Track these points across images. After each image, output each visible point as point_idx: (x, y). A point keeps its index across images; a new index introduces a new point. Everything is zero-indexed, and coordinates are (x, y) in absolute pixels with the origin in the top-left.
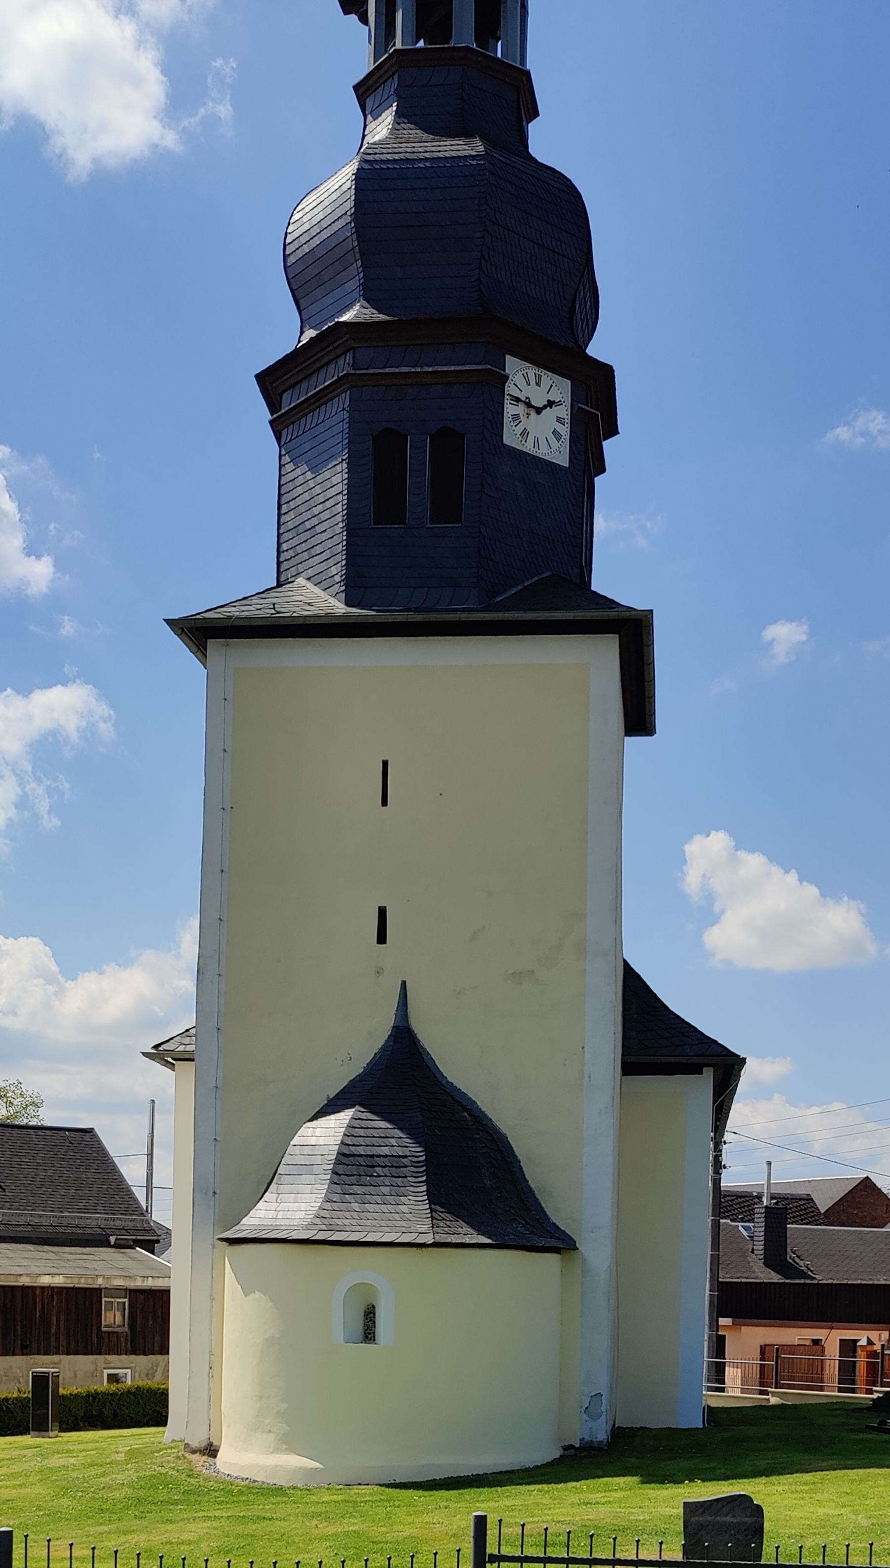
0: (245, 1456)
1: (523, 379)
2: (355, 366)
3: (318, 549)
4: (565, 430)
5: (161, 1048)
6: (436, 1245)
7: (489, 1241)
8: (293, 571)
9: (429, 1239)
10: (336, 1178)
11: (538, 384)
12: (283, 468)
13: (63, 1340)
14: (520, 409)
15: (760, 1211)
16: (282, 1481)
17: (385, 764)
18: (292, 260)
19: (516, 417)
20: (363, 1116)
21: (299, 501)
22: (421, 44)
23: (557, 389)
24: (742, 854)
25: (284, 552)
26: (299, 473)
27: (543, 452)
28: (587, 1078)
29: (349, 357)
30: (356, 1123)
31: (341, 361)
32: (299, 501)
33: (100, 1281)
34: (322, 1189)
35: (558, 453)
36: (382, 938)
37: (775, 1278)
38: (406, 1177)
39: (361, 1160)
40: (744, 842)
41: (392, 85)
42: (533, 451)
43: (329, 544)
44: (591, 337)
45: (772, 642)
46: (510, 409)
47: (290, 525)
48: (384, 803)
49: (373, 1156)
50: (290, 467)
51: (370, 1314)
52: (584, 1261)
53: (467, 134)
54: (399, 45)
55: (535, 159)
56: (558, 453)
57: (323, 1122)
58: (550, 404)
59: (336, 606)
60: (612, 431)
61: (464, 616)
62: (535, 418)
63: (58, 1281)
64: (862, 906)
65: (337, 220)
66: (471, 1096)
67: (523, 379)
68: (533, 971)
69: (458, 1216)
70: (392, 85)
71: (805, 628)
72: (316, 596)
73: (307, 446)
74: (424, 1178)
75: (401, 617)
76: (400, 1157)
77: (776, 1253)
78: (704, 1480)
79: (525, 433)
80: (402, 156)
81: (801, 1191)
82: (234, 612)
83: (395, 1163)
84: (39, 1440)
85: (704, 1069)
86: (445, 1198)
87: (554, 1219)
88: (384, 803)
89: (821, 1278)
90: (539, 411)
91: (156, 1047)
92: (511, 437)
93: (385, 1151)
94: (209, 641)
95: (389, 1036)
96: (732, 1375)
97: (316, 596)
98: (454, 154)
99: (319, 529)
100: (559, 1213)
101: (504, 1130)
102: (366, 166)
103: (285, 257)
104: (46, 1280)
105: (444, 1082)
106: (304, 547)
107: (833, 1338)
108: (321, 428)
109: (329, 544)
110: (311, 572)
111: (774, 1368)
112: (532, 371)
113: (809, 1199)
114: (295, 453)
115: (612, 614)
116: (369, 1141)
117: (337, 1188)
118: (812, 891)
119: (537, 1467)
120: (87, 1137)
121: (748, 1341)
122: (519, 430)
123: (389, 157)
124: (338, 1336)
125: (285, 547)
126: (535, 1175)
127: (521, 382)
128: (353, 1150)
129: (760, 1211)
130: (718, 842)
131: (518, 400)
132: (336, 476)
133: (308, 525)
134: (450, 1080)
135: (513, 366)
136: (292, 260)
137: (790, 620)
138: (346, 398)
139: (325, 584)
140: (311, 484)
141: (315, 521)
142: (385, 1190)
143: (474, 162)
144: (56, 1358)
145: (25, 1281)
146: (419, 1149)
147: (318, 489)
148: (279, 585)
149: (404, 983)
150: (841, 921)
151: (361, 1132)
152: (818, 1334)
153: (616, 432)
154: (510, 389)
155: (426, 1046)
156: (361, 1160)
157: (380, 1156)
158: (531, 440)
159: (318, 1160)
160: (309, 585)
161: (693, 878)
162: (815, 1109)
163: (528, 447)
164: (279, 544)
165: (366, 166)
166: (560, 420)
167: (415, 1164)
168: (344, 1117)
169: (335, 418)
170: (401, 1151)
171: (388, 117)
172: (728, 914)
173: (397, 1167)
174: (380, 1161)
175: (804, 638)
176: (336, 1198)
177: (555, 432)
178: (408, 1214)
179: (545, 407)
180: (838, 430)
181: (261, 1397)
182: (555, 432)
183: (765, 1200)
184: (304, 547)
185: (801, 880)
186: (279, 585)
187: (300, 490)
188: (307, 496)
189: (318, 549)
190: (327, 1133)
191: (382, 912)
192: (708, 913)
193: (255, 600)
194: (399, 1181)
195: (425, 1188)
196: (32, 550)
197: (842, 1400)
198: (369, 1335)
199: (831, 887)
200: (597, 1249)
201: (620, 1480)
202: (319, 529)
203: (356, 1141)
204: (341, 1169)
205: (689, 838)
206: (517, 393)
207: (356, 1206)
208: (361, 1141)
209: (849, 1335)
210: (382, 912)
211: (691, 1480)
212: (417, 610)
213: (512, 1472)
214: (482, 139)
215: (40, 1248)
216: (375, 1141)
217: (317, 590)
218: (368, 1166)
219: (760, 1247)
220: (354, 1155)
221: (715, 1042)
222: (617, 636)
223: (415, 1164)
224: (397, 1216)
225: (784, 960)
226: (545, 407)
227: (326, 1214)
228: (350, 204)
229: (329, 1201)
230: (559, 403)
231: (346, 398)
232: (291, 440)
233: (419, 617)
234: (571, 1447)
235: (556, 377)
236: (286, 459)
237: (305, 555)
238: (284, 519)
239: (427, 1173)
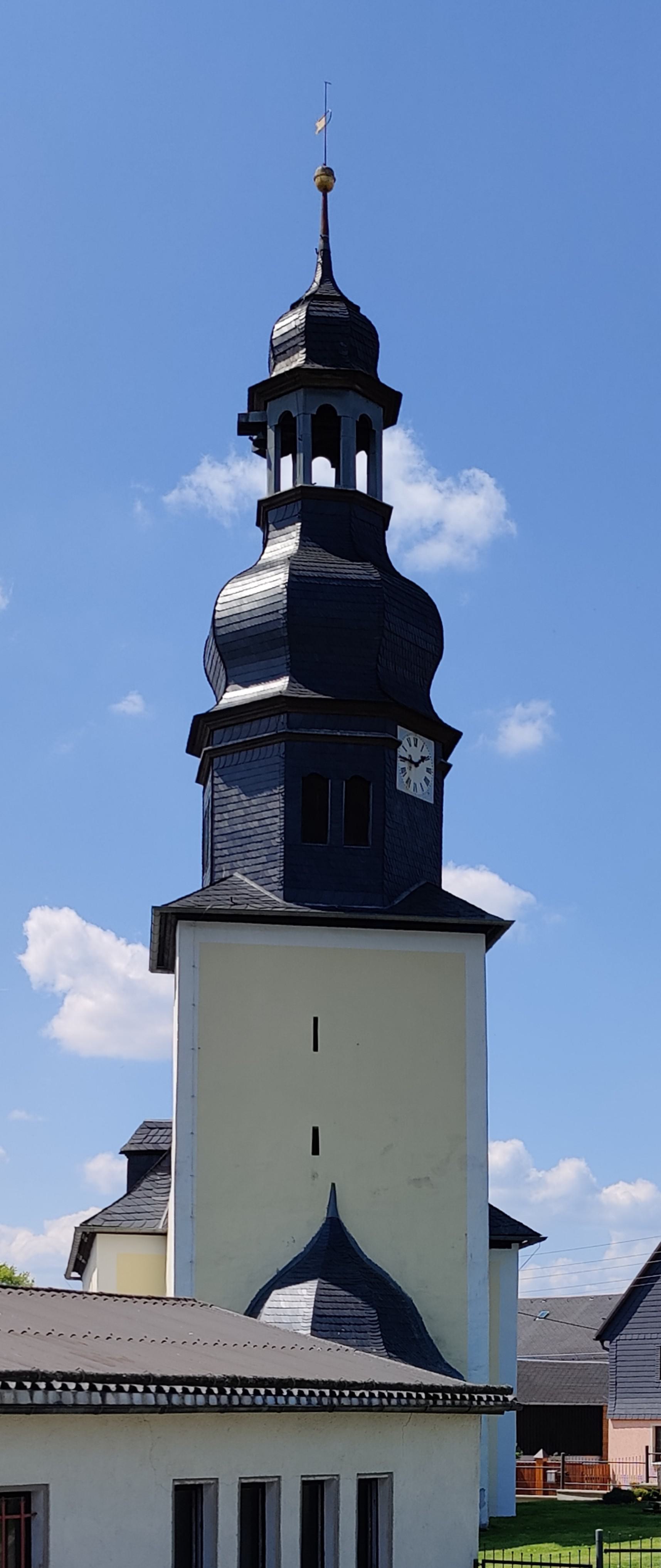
5: (89, 1224)
11: (416, 745)
12: (215, 787)
14: (406, 765)
19: (403, 769)
20: (325, 1286)
25: (218, 850)
27: (419, 794)
28: (469, 1258)
29: (283, 718)
36: (316, 1151)
38: (366, 1332)
46: (401, 764)
48: (316, 1049)
49: (339, 1317)
50: (222, 787)
55: (398, 574)
58: (423, 759)
65: (269, 614)
66: (385, 1270)
68: (428, 1178)
74: (379, 1333)
75: (333, 914)
76: (359, 1317)
80: (320, 574)
85: (513, 1245)
88: (316, 1049)
90: (417, 765)
93: (348, 1313)
94: (179, 922)
95: (324, 1225)
98: (357, 577)
101: (410, 1295)
102: (295, 580)
105: (365, 1259)
112: (412, 736)
115: (486, 921)
122: (405, 779)
123: (310, 574)
128: (325, 1312)
132: (276, 804)
134: (369, 1257)
135: (403, 733)
140: (246, 804)
143: (374, 586)
146: (374, 1311)
149: (333, 1185)
154: (401, 752)
155: (351, 1233)
156: (331, 1319)
157: (344, 1317)
158: (412, 785)
161: (33, 960)
163: (410, 791)
165: (295, 580)
166: (428, 770)
167: (371, 1323)
173: (359, 1325)
174: (346, 1320)
177: (426, 779)
179: (420, 762)
182: (426, 779)
191: (315, 1131)
192: (51, 1002)
195: (381, 1340)
197: (527, 1501)
202: (253, 839)
210: (315, 1131)
218: (336, 1324)
220: (326, 1316)
221: (521, 1224)
222: (483, 936)
223: (371, 1323)
226: (420, 762)
232: (223, 767)
235: (426, 740)
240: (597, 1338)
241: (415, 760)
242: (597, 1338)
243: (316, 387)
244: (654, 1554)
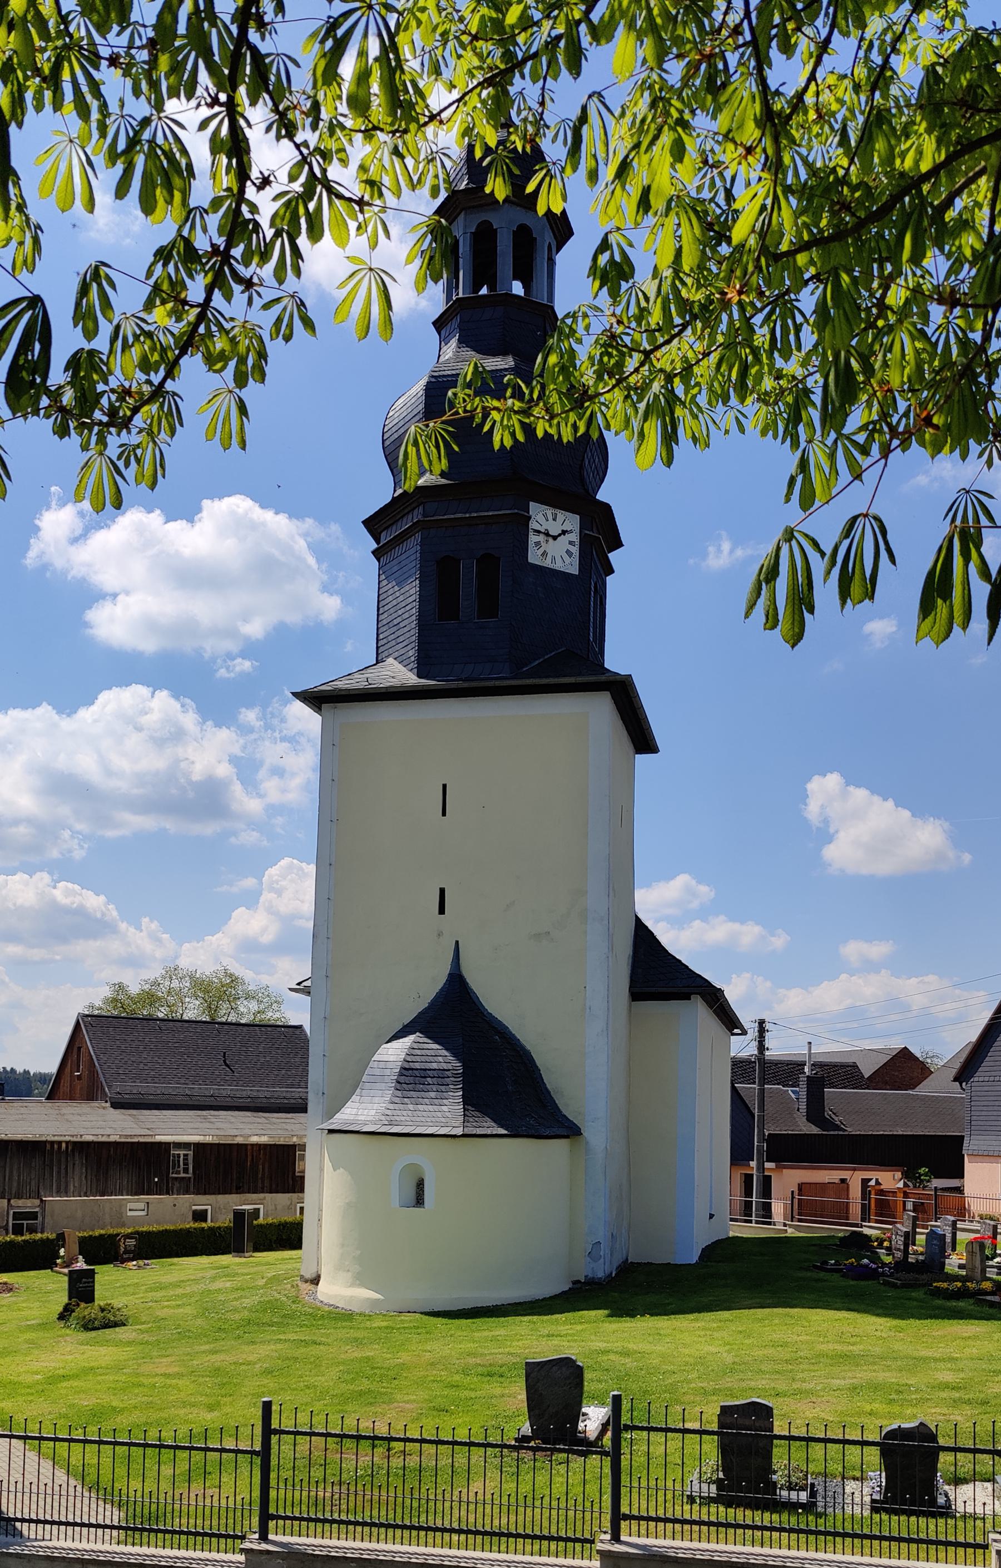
0: (336, 1290)
1: (542, 517)
2: (424, 516)
3: (401, 639)
4: (575, 550)
6: (463, 1136)
7: (502, 1131)
8: (386, 653)
9: (459, 1131)
10: (398, 1086)
11: (554, 520)
13: (267, 1183)
14: (541, 538)
15: (803, 1079)
16: (356, 1309)
17: (444, 786)
18: (387, 443)
20: (421, 1040)
21: (390, 606)
22: (484, 291)
23: (571, 522)
24: (851, 788)
26: (392, 587)
27: (559, 566)
30: (415, 1046)
31: (416, 512)
32: (390, 606)
33: (295, 1139)
34: (388, 1094)
35: (571, 566)
36: (442, 911)
37: (815, 1130)
39: (417, 1073)
40: (851, 780)
41: (455, 322)
42: (551, 566)
43: (408, 635)
44: (602, 481)
45: (871, 634)
46: (533, 538)
47: (385, 622)
48: (444, 814)
51: (420, 1185)
52: (587, 1143)
53: (504, 353)
54: (461, 295)
56: (571, 566)
57: (395, 1044)
58: (564, 532)
59: (411, 679)
60: (616, 543)
61: (498, 683)
62: (553, 541)
63: (264, 1140)
64: (946, 825)
67: (542, 517)
69: (485, 1113)
70: (455, 322)
71: (894, 622)
72: (398, 673)
73: (396, 568)
75: (454, 685)
77: (815, 1111)
78: (652, 1315)
79: (545, 554)
81: (850, 1060)
82: (341, 685)
83: (441, 1075)
84: (238, 1260)
86: (477, 1099)
87: (565, 1112)
88: (444, 814)
89: (851, 1130)
90: (555, 538)
91: (299, 984)
92: (534, 557)
93: (435, 1066)
96: (778, 1209)
97: (398, 673)
99: (402, 625)
100: (568, 1109)
101: (528, 1047)
103: (383, 441)
104: (255, 1139)
106: (393, 637)
107: (855, 1178)
108: (404, 557)
109: (408, 635)
110: (396, 654)
111: (807, 1204)
112: (549, 511)
113: (854, 1066)
114: (389, 573)
116: (423, 1059)
117: (399, 1094)
118: (906, 814)
119: (544, 1299)
120: (298, 1032)
121: (787, 1180)
124: (396, 1203)
125: (381, 636)
126: (550, 1081)
127: (540, 518)
129: (803, 1079)
130: (833, 781)
131: (539, 532)
132: (412, 590)
133: (395, 622)
136: (387, 443)
137: (881, 618)
138: (418, 536)
139: (405, 663)
141: (399, 619)
142: (433, 1094)
144: (262, 1195)
145: (239, 1140)
147: (401, 598)
148: (378, 662)
149: (457, 942)
150: (927, 838)
151: (419, 1052)
152: (845, 1175)
153: (612, 572)
154: (533, 525)
156: (417, 1073)
159: (388, 1072)
160: (396, 663)
161: (813, 809)
162: (914, 981)
163: (547, 563)
164: (378, 635)
166: (571, 543)
167: (455, 1076)
168: (408, 1041)
169: (411, 551)
170: (445, 1066)
171: (454, 343)
172: (842, 835)
174: (430, 1073)
175: (894, 629)
176: (397, 1100)
177: (568, 552)
178: (445, 1112)
180: (919, 478)
181: (343, 1245)
182: (568, 552)
183: (806, 1070)
184: (393, 637)
185: (897, 806)
186: (378, 662)
187: (391, 598)
188: (395, 602)
189: (401, 639)
190: (395, 1052)
191: (442, 891)
192: (825, 836)
193: (356, 676)
194: (443, 1088)
196: (326, 589)
198: (419, 1201)
199: (919, 812)
200: (597, 1134)
201: (593, 1313)
202: (402, 625)
203: (414, 1059)
204: (402, 1079)
205: (809, 779)
206: (538, 527)
207: (411, 1107)
208: (418, 1058)
209: (867, 1175)
210: (442, 891)
211: (642, 1315)
212: (465, 680)
213: (520, 1304)
214: (514, 355)
215: (256, 1114)
216: (427, 1059)
217: (400, 666)
219: (803, 1107)
223: (455, 1076)
224: (439, 1114)
225: (884, 868)
227: (389, 1112)
228: (422, 406)
229: (393, 1103)
230: (571, 532)
231: (418, 536)
233: (466, 685)
234: (578, 1282)
236: (383, 577)
237: (394, 643)
238: (381, 617)
239: (464, 1082)
240: (955, 1080)
241: (554, 532)
242: (955, 1080)
243: (474, 207)
244: (224, 1455)
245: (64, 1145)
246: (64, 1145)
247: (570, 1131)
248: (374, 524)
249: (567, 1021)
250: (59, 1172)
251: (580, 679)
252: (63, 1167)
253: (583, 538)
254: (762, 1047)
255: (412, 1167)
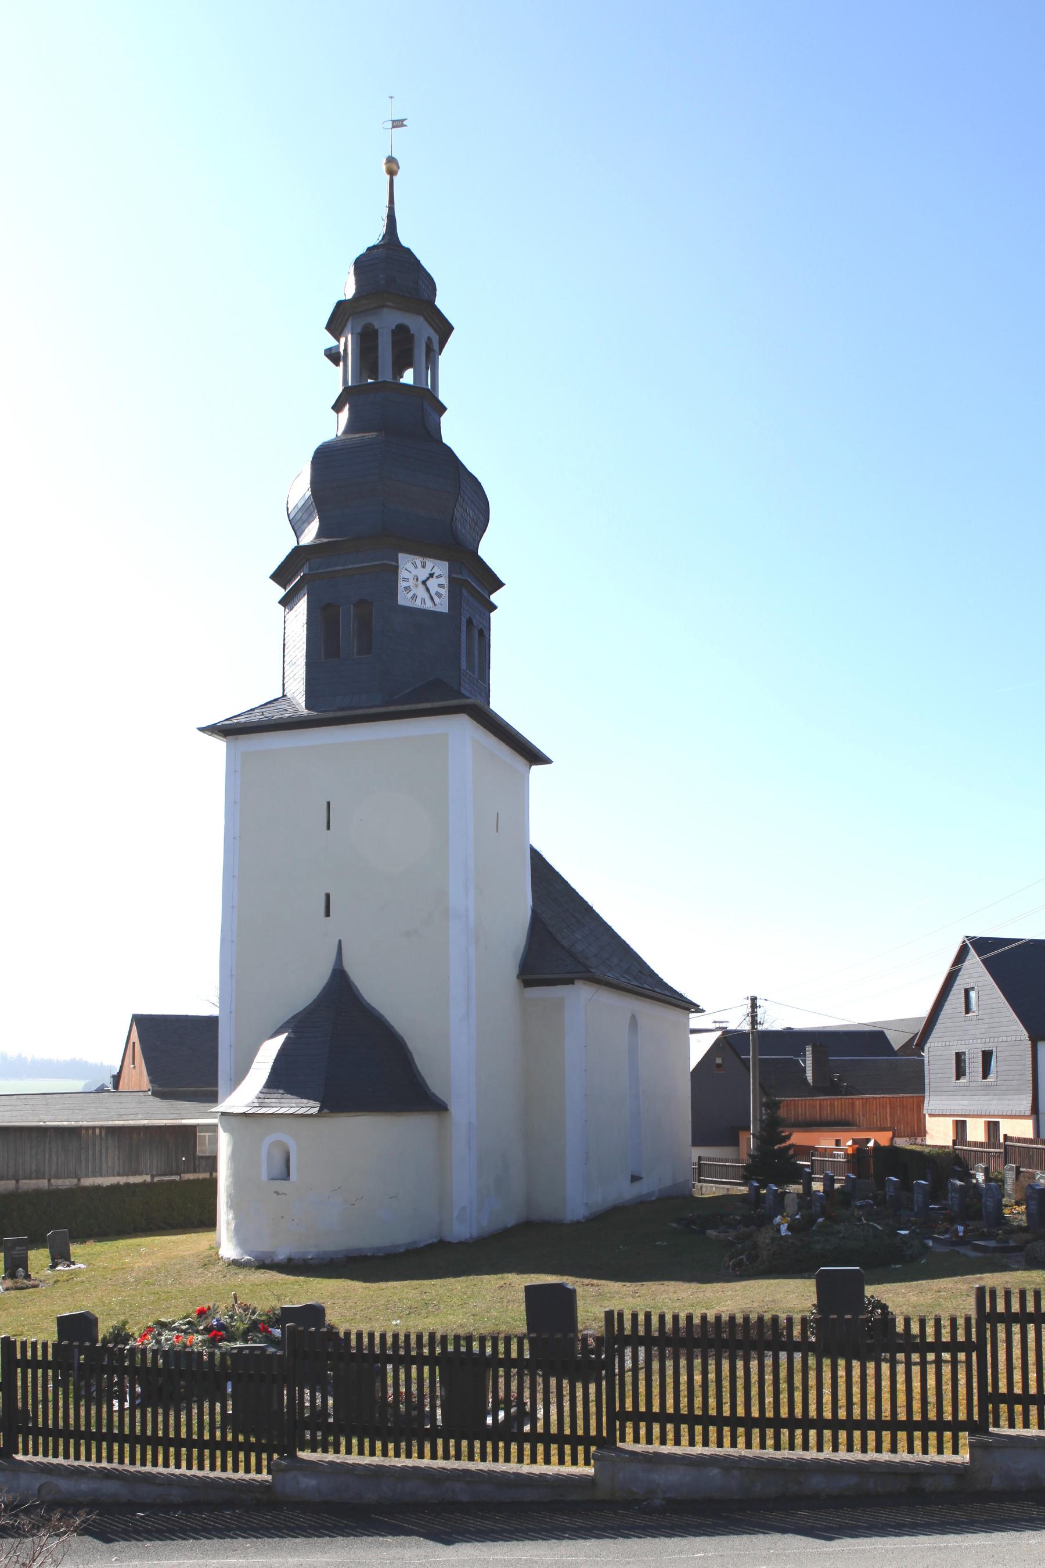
23: (441, 568)
75: (330, 715)
112: (418, 560)
124: (264, 1176)
149: (340, 941)
166: (440, 586)
191: (328, 896)
210: (328, 896)
245: (97, 1131)
246: (97, 1131)
247: (435, 1105)
248: (280, 576)
249: (453, 1004)
250: (94, 1155)
251: (428, 705)
252: (97, 1149)
253: (451, 580)
254: (754, 1022)
255: (278, 1143)
